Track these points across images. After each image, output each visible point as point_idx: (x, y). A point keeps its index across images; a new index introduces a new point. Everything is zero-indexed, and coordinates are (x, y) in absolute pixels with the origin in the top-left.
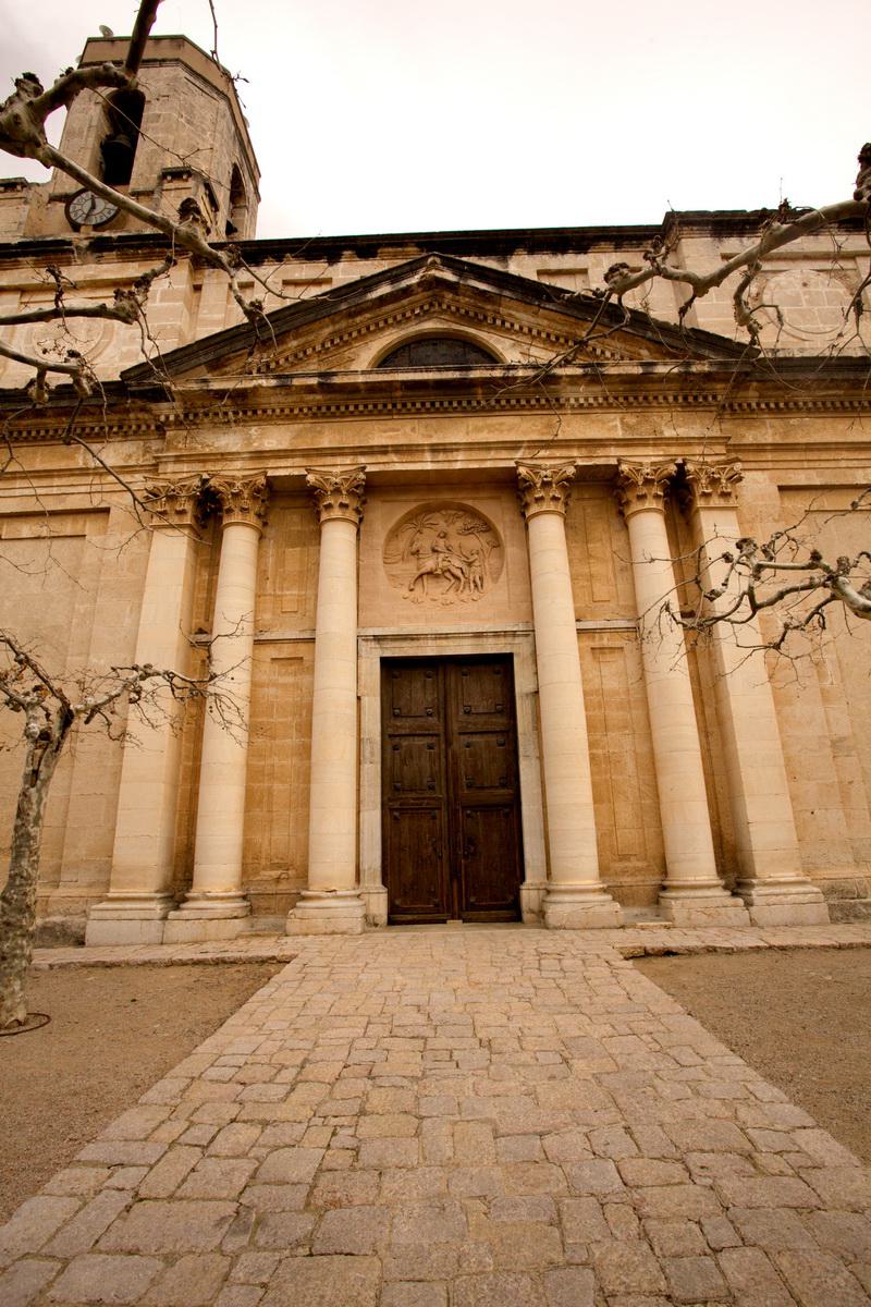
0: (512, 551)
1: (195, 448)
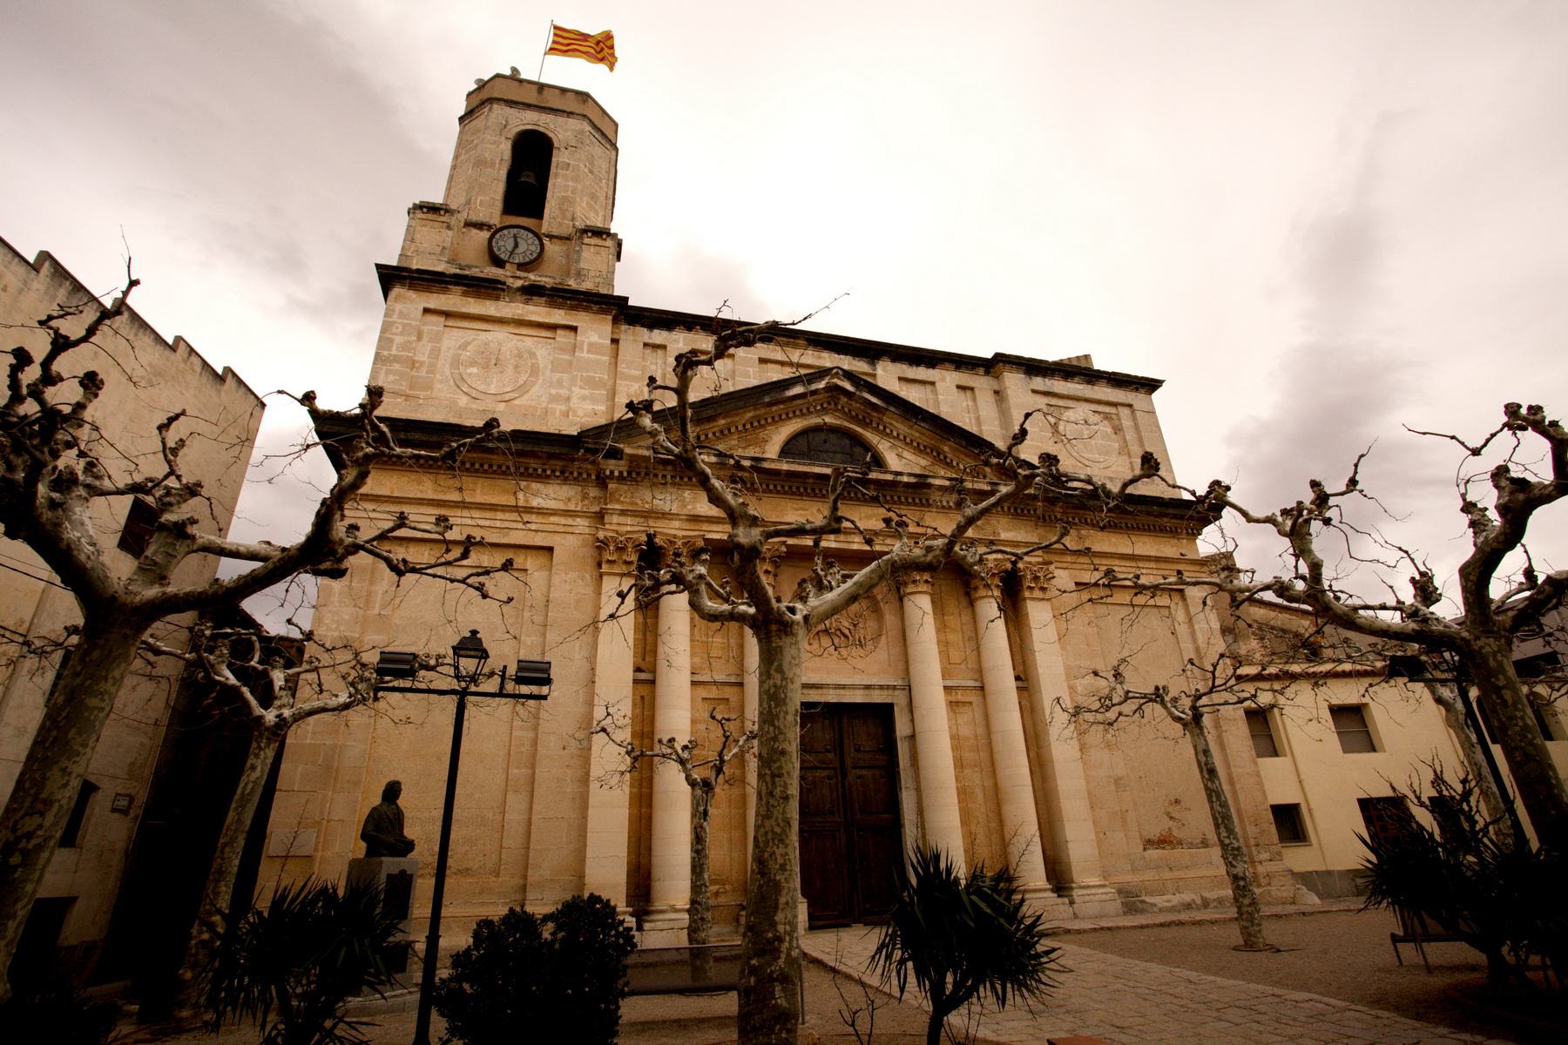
0: (890, 619)
1: (637, 504)
